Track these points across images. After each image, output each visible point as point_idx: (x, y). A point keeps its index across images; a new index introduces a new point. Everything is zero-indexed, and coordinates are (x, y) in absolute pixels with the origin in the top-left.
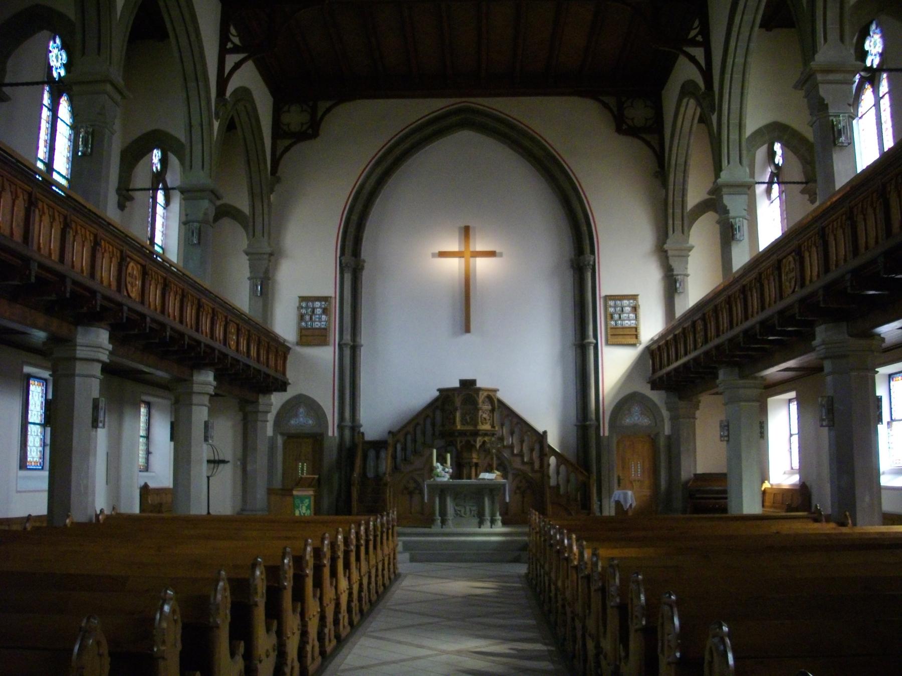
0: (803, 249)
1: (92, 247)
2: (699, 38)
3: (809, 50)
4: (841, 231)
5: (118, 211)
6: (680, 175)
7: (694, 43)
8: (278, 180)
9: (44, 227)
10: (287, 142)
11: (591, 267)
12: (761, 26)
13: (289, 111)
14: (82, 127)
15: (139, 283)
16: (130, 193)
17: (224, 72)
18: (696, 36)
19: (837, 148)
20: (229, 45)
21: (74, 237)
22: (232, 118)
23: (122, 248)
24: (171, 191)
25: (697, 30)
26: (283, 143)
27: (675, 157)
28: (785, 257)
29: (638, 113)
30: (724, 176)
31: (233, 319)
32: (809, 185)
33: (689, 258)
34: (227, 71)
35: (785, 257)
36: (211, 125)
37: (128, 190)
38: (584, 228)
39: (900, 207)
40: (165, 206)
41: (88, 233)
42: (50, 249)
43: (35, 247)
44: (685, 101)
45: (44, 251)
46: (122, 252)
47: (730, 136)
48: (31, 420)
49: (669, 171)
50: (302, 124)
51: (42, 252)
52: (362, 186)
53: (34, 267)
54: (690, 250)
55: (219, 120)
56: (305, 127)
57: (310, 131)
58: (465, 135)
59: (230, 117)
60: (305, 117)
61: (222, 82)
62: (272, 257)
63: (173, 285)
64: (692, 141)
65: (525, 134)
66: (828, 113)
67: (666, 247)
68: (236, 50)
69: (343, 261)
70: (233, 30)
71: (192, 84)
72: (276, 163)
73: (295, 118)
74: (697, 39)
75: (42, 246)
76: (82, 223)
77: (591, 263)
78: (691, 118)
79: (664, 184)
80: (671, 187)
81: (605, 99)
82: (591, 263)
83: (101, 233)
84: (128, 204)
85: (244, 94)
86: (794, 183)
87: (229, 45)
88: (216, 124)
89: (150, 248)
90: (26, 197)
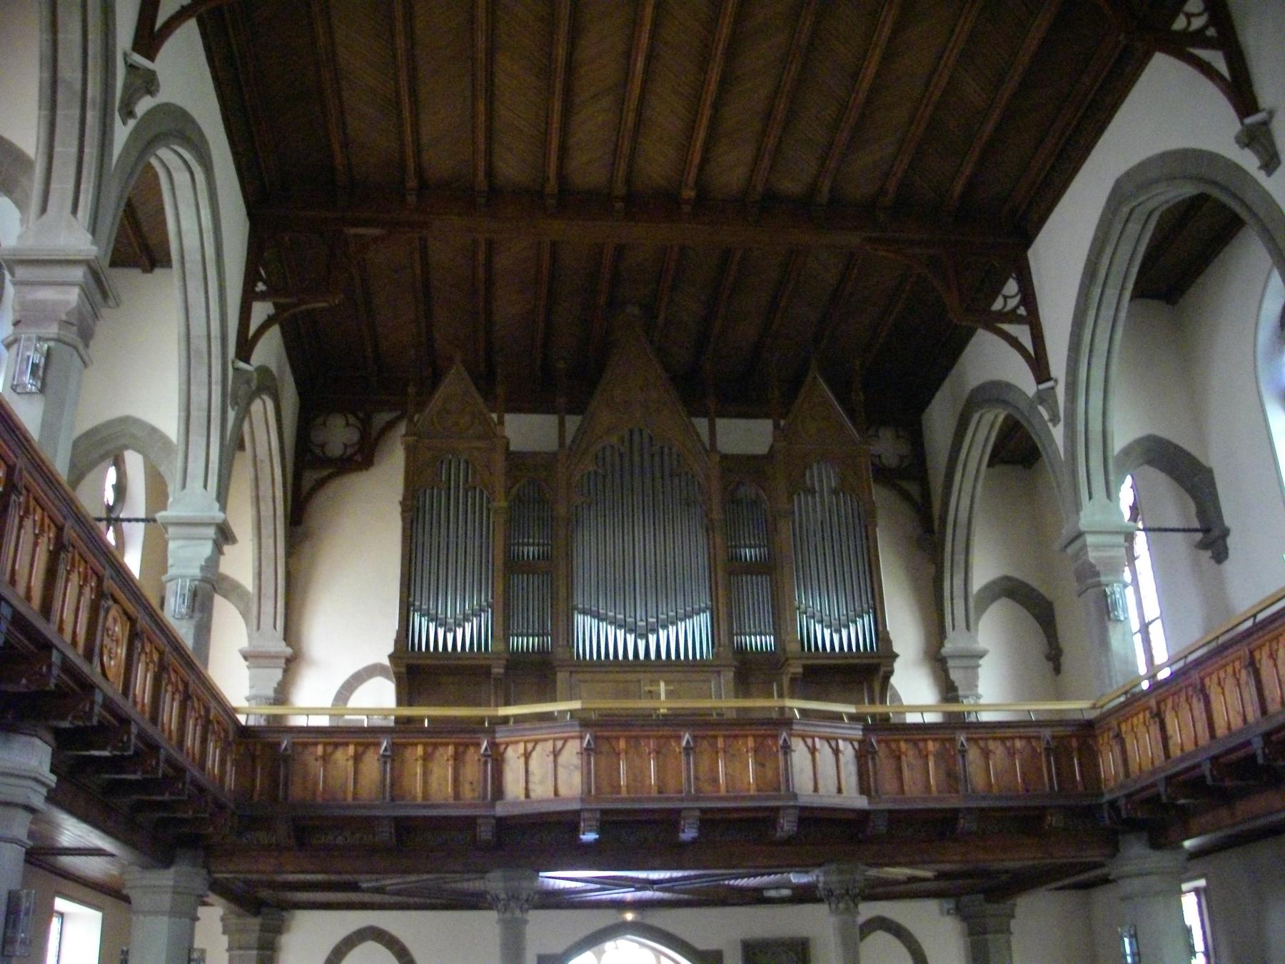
1: (49, 551)
2: (1022, 311)
7: (1012, 317)
15: (122, 652)
17: (248, 332)
29: (888, 447)
33: (980, 670)
48: (925, 714)
54: (981, 657)
60: (352, 436)
78: (982, 443)
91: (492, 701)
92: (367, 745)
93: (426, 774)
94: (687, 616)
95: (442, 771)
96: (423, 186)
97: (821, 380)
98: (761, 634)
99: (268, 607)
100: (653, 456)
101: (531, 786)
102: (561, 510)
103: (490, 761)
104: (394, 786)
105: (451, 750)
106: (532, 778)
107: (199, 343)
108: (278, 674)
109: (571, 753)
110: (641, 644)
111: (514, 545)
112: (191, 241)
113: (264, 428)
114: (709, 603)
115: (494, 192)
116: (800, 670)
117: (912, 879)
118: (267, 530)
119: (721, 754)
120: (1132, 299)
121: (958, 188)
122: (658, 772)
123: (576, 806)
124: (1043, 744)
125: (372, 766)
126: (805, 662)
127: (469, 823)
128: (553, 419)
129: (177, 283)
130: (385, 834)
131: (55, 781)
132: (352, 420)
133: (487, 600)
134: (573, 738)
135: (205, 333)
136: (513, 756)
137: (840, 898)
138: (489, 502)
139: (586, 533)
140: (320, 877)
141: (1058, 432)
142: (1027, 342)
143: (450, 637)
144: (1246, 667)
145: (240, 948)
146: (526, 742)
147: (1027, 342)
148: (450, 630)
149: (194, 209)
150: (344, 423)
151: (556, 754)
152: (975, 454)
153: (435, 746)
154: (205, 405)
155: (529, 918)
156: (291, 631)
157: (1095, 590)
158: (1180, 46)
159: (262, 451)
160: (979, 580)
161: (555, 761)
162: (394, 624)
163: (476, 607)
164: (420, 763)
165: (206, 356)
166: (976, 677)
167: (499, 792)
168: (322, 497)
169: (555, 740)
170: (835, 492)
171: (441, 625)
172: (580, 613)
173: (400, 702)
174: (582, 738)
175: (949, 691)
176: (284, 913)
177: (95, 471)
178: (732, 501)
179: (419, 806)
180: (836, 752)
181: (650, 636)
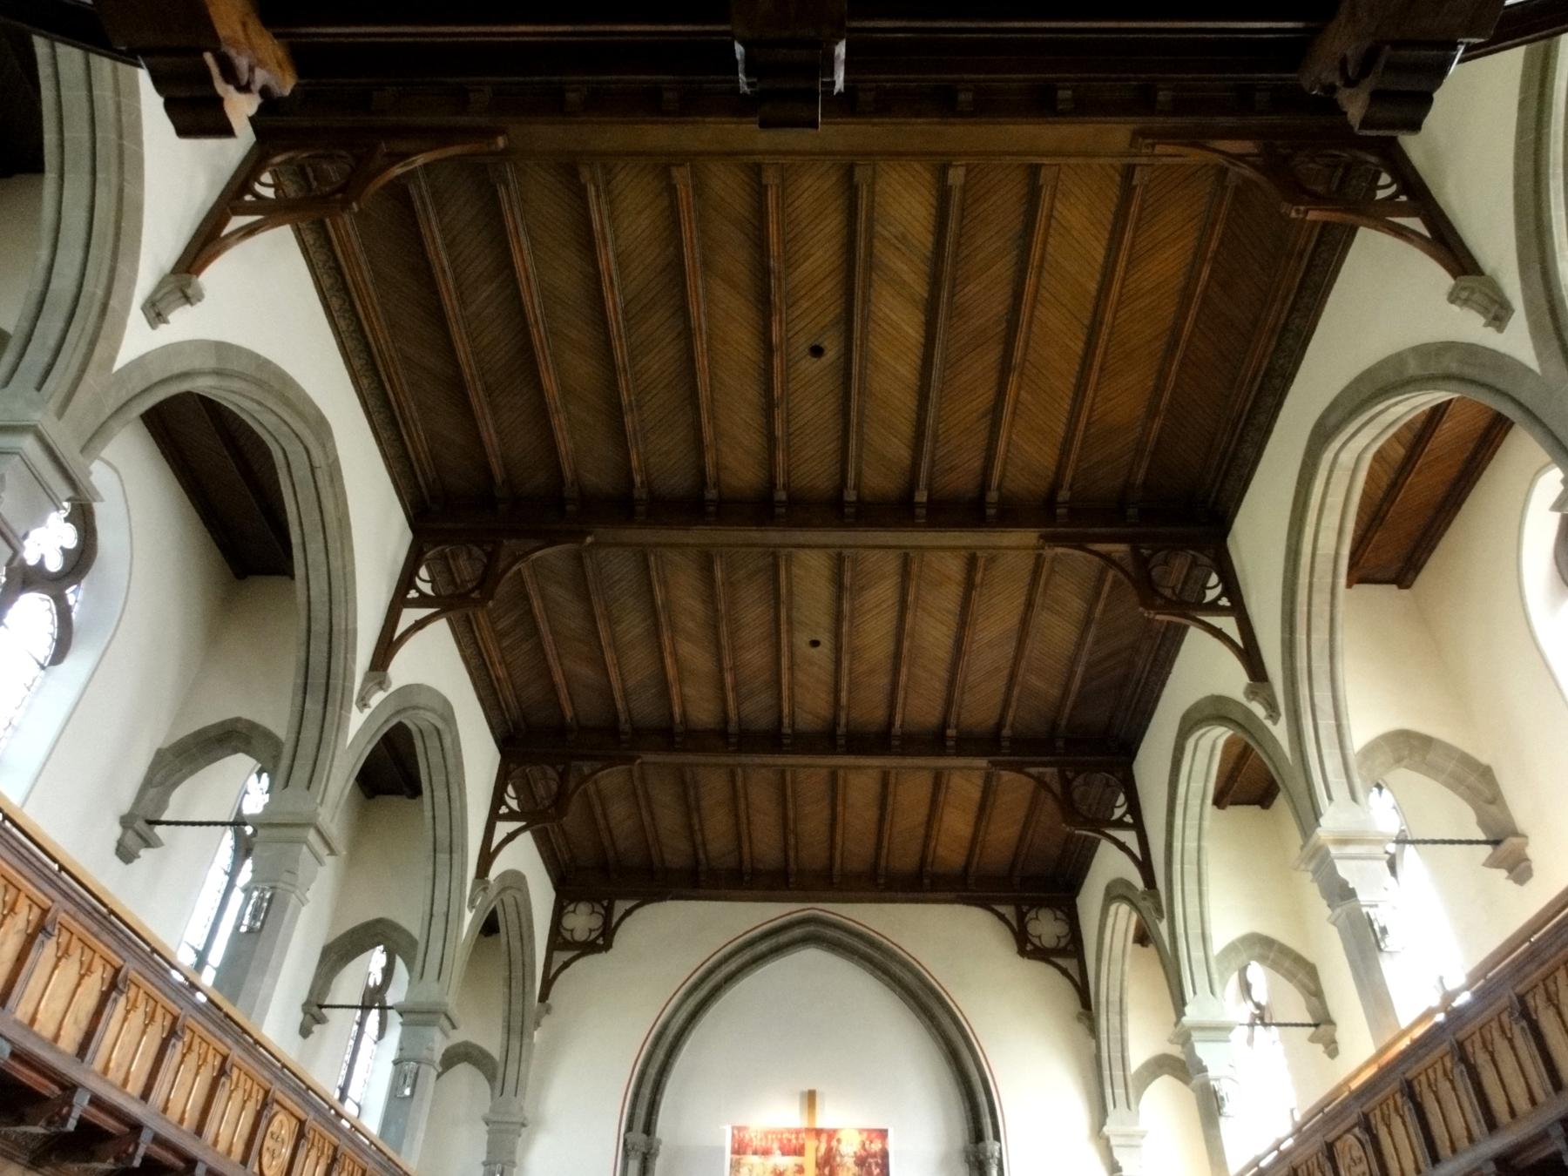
2: (1128, 819)
3: (1309, 816)
4: (1448, 1085)
5: (299, 1038)
6: (1115, 1020)
7: (1120, 824)
8: (548, 1010)
9: (128, 1032)
10: (567, 955)
11: (996, 1161)
13: (574, 912)
14: (256, 889)
15: (286, 1152)
16: (324, 1010)
18: (1124, 815)
19: (1385, 955)
20: (504, 810)
21: (184, 1055)
22: (494, 913)
24: (390, 1012)
26: (561, 957)
27: (1105, 988)
28: (1339, 1138)
29: (1046, 928)
30: (1192, 1014)
32: (1322, 1028)
34: (553, 971)
35: (1339, 1138)
36: (460, 917)
37: (321, 1007)
38: (982, 1099)
40: (375, 1039)
41: (211, 1052)
42: (128, 1073)
43: (98, 1065)
44: (1113, 908)
45: (115, 1075)
47: (1191, 955)
49: (1098, 1013)
50: (591, 931)
51: (110, 1076)
52: (665, 1026)
53: (81, 1102)
54: (1143, 1137)
55: (474, 910)
56: (594, 935)
57: (600, 941)
58: (811, 956)
59: (491, 908)
60: (596, 922)
61: (487, 858)
62: (524, 1129)
63: (347, 1161)
64: (1127, 967)
65: (892, 955)
66: (1357, 900)
67: (1105, 1129)
68: (512, 816)
69: (629, 1141)
70: (510, 790)
71: (443, 857)
72: (548, 983)
73: (581, 922)
75: (112, 1065)
76: (205, 1034)
77: (997, 1154)
79: (1093, 1030)
80: (1103, 1036)
81: (1002, 909)
82: (997, 1154)
83: (236, 1054)
84: (316, 1028)
85: (515, 880)
86: (1296, 1025)
87: (504, 810)
88: (469, 916)
89: (338, 1106)
120: (1349, 585)
144: (1516, 1020)
147: (1135, 847)
149: (322, 705)
158: (1380, 217)
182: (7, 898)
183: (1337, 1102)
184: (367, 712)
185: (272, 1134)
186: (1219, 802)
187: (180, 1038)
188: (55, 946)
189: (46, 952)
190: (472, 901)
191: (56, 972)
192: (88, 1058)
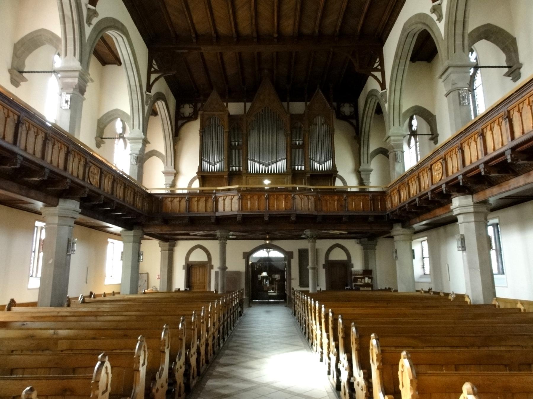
0: (447, 157)
2: (379, 67)
7: (376, 70)
12: (410, 60)
15: (98, 177)
18: (378, 66)
23: (46, 131)
25: (378, 63)
29: (347, 109)
31: (92, 161)
34: (152, 81)
39: (532, 114)
43: (23, 146)
46: (68, 148)
51: (74, 175)
54: (371, 171)
68: (156, 72)
70: (154, 62)
74: (378, 68)
87: (153, 69)
90: (43, 135)
91: (225, 184)
92: (182, 198)
93: (198, 205)
94: (280, 161)
95: (202, 204)
96: (197, 36)
97: (320, 92)
98: (300, 165)
99: (169, 159)
100: (271, 115)
101: (225, 208)
102: (245, 131)
103: (188, 201)
104: (189, 209)
105: (204, 199)
106: (225, 206)
107: (133, 87)
108: (172, 178)
109: (235, 199)
110: (267, 169)
111: (232, 141)
112: (126, 57)
113: (163, 109)
114: (286, 157)
115: (218, 37)
116: (310, 176)
117: (341, 234)
118: (168, 138)
119: (276, 200)
121: (359, 28)
122: (258, 204)
123: (236, 213)
124: (369, 198)
125: (184, 203)
126: (311, 173)
127: (209, 218)
128: (242, 104)
129: (124, 70)
130: (213, 220)
131: (78, 208)
132: (191, 106)
133: (223, 157)
134: (236, 195)
135: (134, 84)
136: (221, 200)
137: (311, 238)
138: (224, 130)
139: (252, 138)
140: (185, 232)
141: (386, 105)
142: (380, 78)
143: (213, 167)
145: (164, 251)
146: (224, 196)
148: (213, 166)
150: (183, 109)
151: (231, 199)
152: (370, 111)
153: (201, 198)
154: (137, 105)
155: (227, 242)
156: (176, 166)
157: (393, 153)
159: (164, 116)
160: (372, 148)
161: (231, 201)
162: (198, 164)
163: (220, 159)
164: (196, 202)
165: (136, 91)
166: (369, 177)
167: (217, 209)
168: (184, 128)
169: (231, 196)
170: (323, 124)
171: (211, 164)
172: (249, 160)
173: (200, 186)
174: (238, 195)
175: (361, 182)
176: (176, 241)
177: (112, 123)
178: (293, 127)
179: (196, 213)
180: (309, 199)
181: (269, 166)
182: (43, 135)
183: (202, 329)
184: (92, 27)
185: (91, 172)
186: (414, 59)
187: (71, 153)
188: (25, 127)
189: (71, 158)
190: (147, 102)
191: (60, 154)
192: (45, 159)
